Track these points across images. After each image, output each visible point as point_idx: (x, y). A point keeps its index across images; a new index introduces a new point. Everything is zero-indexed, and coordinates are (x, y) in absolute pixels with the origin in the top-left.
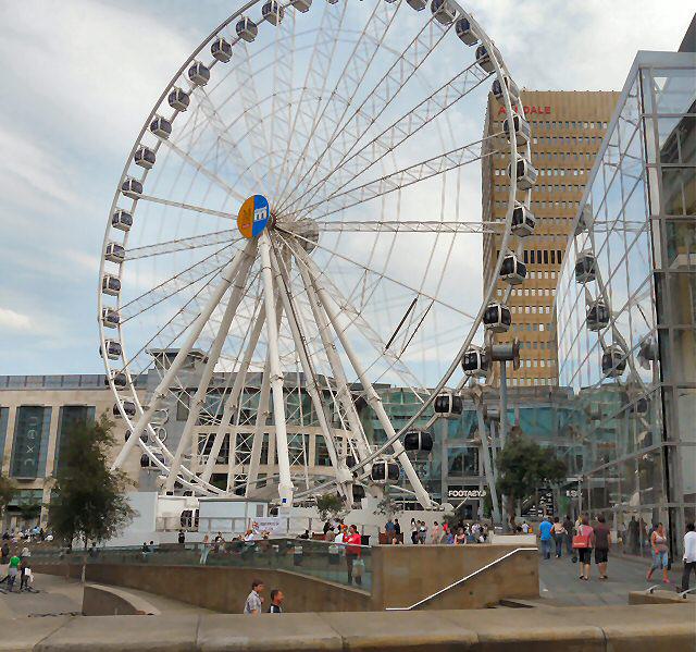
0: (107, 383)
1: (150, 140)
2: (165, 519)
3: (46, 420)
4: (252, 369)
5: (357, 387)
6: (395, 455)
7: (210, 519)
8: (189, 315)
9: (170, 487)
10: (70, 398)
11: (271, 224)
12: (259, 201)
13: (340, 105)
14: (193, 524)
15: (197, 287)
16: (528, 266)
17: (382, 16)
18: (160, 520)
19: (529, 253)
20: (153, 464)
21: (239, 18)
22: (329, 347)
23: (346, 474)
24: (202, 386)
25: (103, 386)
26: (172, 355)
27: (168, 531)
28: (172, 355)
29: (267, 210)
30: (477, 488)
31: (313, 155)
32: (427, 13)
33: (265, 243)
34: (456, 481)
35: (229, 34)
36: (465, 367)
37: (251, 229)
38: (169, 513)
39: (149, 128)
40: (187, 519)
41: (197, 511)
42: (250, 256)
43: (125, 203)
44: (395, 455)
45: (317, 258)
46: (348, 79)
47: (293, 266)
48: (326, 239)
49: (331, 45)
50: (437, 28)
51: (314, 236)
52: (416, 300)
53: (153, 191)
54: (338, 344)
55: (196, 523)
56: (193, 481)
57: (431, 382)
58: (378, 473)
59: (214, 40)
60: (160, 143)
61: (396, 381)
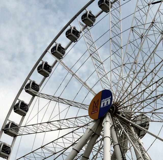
1: (50, 59)
15: (62, 133)
33: (108, 124)
37: (98, 113)
39: (50, 50)
43: (25, 97)
45: (146, 141)
46: (123, 93)
52: (153, 4)
53: (156, 35)
60: (56, 61)
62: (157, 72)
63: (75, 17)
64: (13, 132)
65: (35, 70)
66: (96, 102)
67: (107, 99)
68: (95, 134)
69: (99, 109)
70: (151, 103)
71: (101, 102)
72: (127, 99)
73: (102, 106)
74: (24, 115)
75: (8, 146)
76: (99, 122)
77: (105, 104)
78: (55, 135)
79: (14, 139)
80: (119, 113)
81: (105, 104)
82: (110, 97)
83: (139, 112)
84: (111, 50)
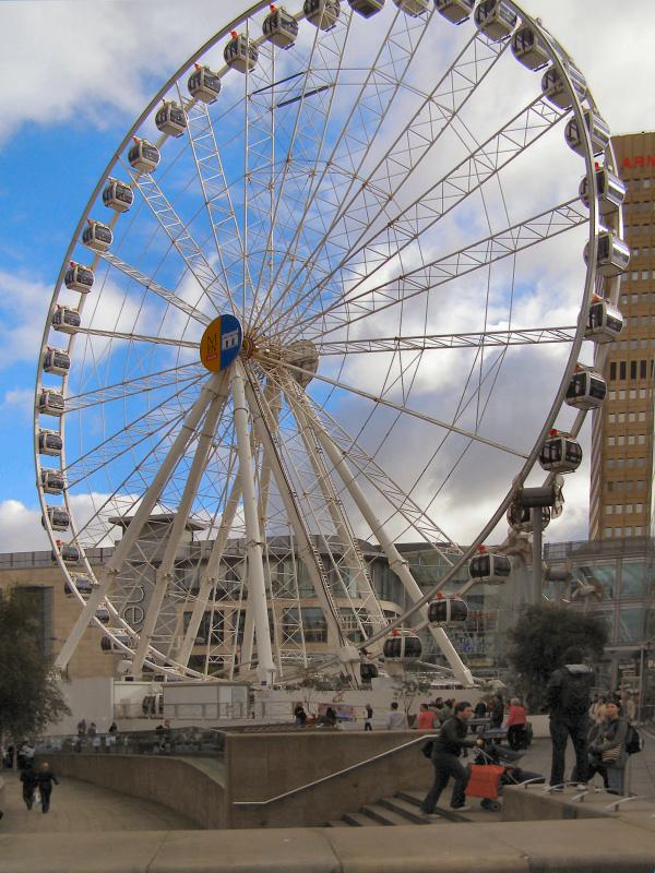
0: (54, 558)
4: (232, 535)
7: (176, 706)
11: (246, 349)
14: (157, 711)
17: (401, 39)
18: (119, 707)
19: (638, 365)
20: (116, 647)
21: (192, 69)
22: (333, 506)
25: (51, 563)
27: (127, 718)
32: (470, 26)
35: (179, 95)
38: (128, 700)
40: (150, 706)
41: (161, 698)
47: (284, 405)
48: (327, 366)
50: (484, 47)
51: (311, 362)
52: (279, 106)
54: (347, 498)
55: (161, 709)
56: (166, 665)
61: (414, 538)
62: (371, 80)
66: (212, 337)
68: (218, 396)
69: (218, 350)
72: (267, 324)
73: (224, 346)
77: (230, 344)
80: (257, 350)
81: (230, 344)
82: (237, 331)
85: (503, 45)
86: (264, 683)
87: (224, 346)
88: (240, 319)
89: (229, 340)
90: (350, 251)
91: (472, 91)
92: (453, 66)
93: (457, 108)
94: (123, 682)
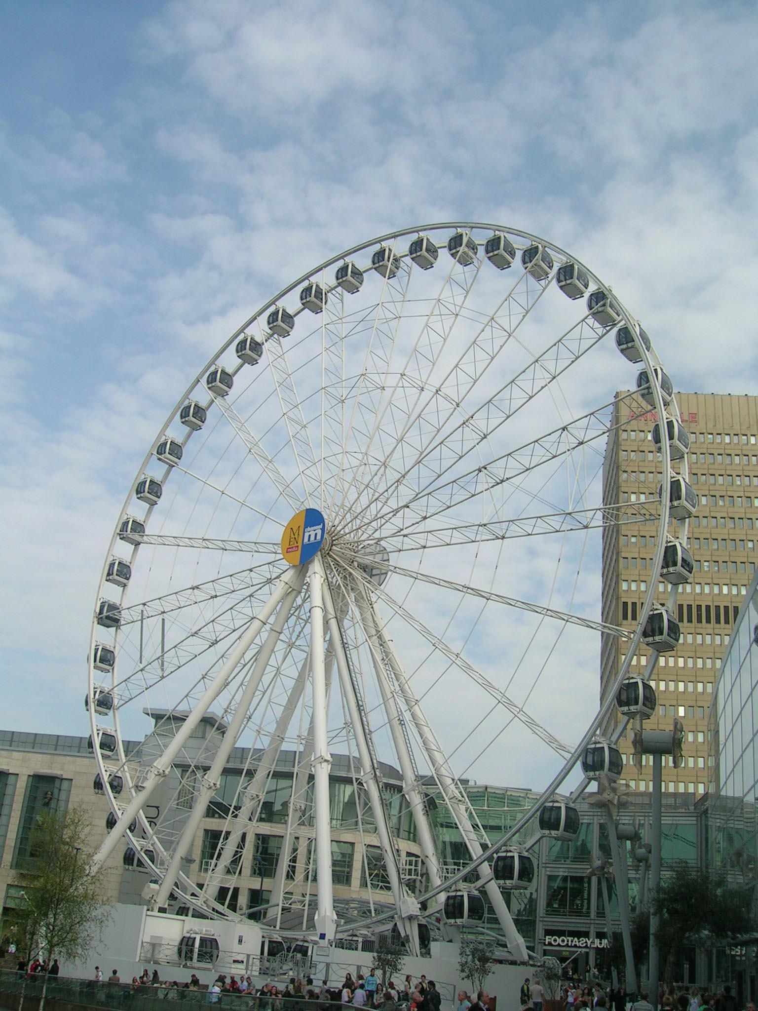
0: (91, 745)
2: (154, 946)
3: (9, 790)
5: (428, 781)
6: (479, 883)
8: (208, 636)
9: (162, 900)
10: (40, 764)
12: (313, 517)
13: (446, 407)
16: (684, 626)
21: (305, 284)
23: (410, 905)
24: (218, 765)
26: (180, 719)
28: (180, 719)
29: (323, 530)
30: (586, 935)
31: (397, 463)
34: (558, 922)
36: (586, 767)
38: (161, 938)
39: (204, 381)
42: (300, 587)
44: (479, 883)
49: (448, 323)
57: (539, 786)
58: (453, 908)
59: (272, 309)
63: (254, 319)
64: (136, 537)
65: (176, 416)
67: (315, 528)
69: (300, 544)
70: (391, 518)
71: (304, 532)
73: (306, 540)
74: (153, 504)
75: (156, 481)
76: (302, 567)
77: (312, 538)
78: (209, 611)
79: (124, 589)
81: (312, 538)
82: (321, 526)
83: (372, 538)
84: (324, 367)
85: (605, 331)
86: (323, 936)
87: (306, 540)
88: (325, 516)
89: (313, 533)
90: (422, 453)
91: (573, 362)
92: (561, 339)
93: (557, 373)
94: (156, 913)
